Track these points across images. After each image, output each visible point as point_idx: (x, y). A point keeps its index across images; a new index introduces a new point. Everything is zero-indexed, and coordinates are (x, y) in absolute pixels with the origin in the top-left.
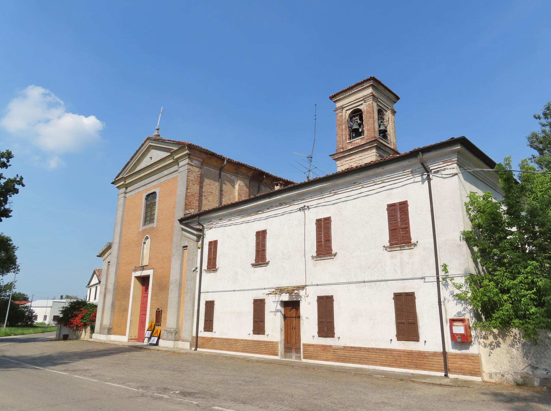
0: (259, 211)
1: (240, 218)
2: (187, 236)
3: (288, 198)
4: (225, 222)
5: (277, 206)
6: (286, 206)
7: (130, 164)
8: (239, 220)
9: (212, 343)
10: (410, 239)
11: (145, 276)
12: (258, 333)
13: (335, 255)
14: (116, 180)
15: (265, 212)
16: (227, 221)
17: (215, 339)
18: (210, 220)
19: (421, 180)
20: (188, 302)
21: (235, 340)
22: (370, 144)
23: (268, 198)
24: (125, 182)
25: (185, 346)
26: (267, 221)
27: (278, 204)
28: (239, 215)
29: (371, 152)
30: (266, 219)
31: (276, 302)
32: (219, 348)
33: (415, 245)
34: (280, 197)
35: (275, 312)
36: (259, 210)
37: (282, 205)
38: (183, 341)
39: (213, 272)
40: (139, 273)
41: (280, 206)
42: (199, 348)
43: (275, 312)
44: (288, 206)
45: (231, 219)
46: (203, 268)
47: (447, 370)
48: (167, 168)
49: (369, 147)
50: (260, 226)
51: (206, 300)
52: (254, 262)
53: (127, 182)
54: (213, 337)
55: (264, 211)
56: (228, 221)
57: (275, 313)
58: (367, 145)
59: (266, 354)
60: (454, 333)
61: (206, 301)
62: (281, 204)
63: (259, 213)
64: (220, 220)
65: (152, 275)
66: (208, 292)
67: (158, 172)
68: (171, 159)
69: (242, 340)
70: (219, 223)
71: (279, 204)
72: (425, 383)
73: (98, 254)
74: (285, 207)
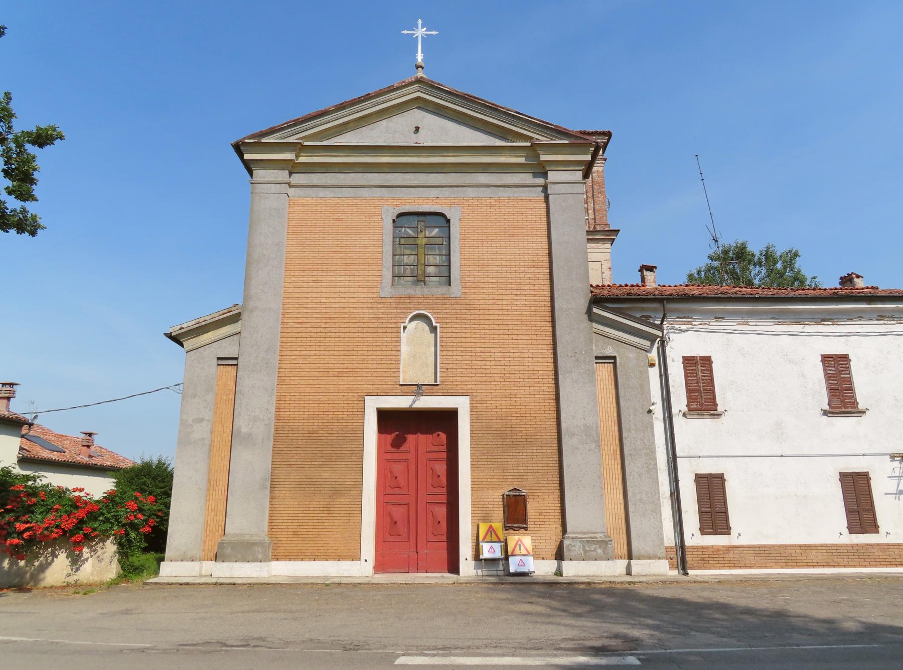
1: (772, 324)
2: (611, 336)
4: (730, 325)
5: (871, 319)
6: (889, 322)
7: (328, 118)
10: (856, 403)
11: (442, 410)
13: (719, 415)
14: (264, 140)
15: (839, 323)
16: (735, 324)
18: (686, 316)
21: (800, 546)
22: (607, 233)
23: (865, 303)
24: (297, 157)
25: (662, 569)
26: (847, 340)
27: (875, 316)
28: (772, 318)
29: (602, 246)
30: (841, 336)
31: (897, 478)
32: (757, 565)
33: (863, 412)
34: (894, 306)
35: (896, 494)
37: (883, 320)
38: (639, 559)
39: (712, 417)
41: (877, 320)
42: (693, 568)
43: (896, 494)
44: (893, 322)
45: (748, 322)
46: (675, 411)
49: (604, 237)
50: (835, 347)
52: (827, 408)
53: (302, 159)
55: (837, 322)
56: (737, 325)
57: (897, 495)
58: (602, 233)
60: (667, 561)
61: (696, 475)
63: (825, 323)
64: (716, 318)
66: (700, 457)
69: (821, 545)
70: (711, 324)
71: (878, 316)
73: (175, 330)
74: (887, 323)
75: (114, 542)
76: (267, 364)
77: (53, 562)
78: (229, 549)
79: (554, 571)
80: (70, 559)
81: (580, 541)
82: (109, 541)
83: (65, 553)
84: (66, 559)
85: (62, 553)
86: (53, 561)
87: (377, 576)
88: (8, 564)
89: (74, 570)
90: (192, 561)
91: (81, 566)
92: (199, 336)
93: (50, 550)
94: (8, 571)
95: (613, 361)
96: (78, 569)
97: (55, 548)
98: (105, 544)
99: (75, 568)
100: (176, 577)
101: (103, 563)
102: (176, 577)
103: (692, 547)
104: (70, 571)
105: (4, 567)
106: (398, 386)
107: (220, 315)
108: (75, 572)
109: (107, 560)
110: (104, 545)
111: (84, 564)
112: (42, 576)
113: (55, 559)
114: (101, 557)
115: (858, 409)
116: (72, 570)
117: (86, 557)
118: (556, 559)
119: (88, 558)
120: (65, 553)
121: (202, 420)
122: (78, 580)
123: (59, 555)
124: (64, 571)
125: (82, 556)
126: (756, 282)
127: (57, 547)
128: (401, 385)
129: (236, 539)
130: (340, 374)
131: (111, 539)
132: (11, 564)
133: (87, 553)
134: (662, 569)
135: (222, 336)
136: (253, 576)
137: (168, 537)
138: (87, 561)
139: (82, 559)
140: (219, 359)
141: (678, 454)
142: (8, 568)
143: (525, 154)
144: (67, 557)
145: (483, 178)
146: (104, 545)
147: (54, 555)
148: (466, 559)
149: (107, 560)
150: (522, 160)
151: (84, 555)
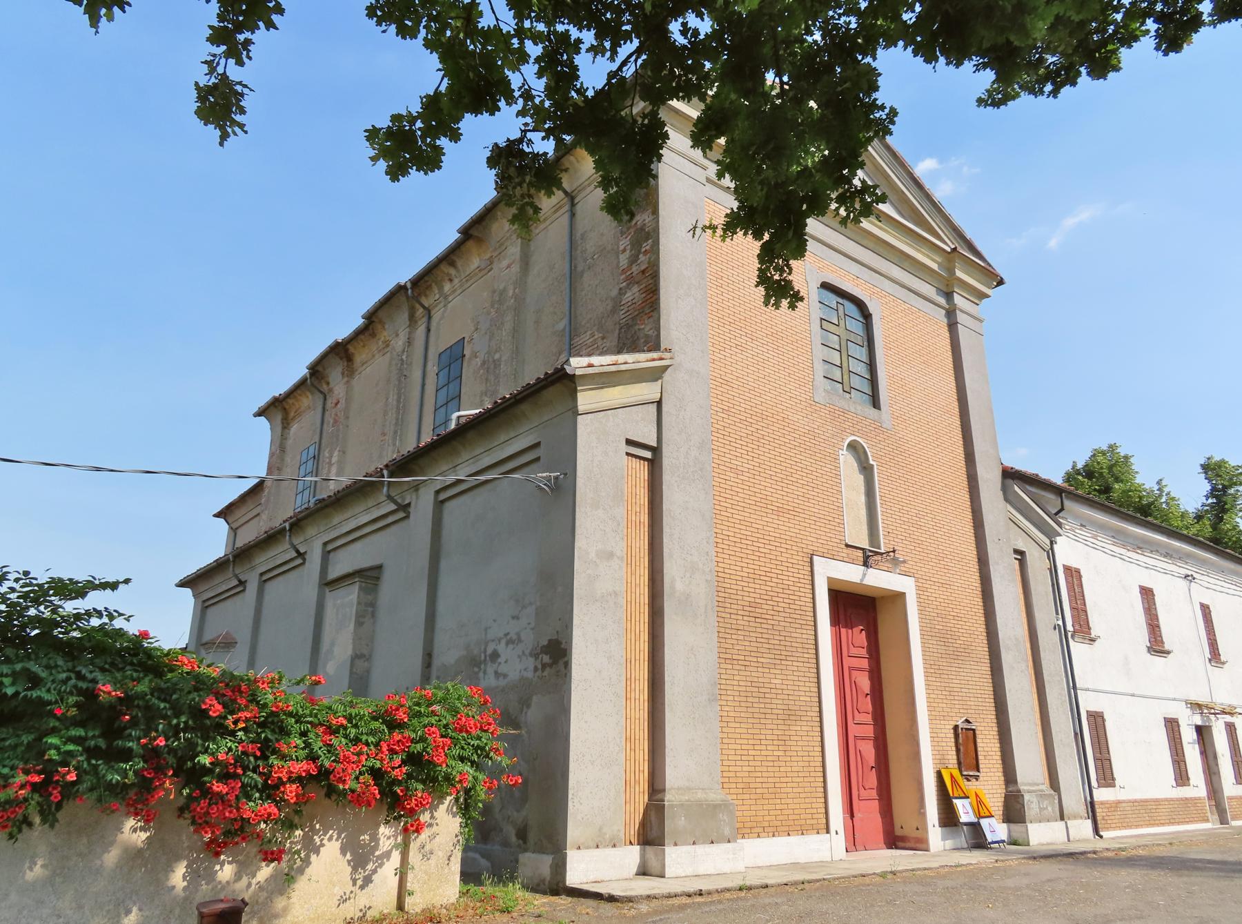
0: (1140, 548)
3: (1178, 551)
8: (1106, 543)
9: (1119, 813)
12: (1183, 785)
15: (1146, 554)
17: (1124, 805)
19: (579, 417)
20: (1057, 709)
28: (1113, 537)
33: (1168, 653)
36: (1141, 546)
40: (851, 573)
47: (1223, 820)
48: (906, 265)
51: (1166, 716)
54: (1118, 798)
59: (1197, 822)
62: (1167, 555)
64: (1082, 525)
65: (914, 592)
67: (871, 245)
68: (933, 260)
69: (1166, 800)
72: (1160, 844)
75: (455, 809)
76: (701, 470)
77: (307, 866)
78: (683, 818)
79: (635, 870)
80: (348, 856)
81: (1036, 795)
82: (443, 808)
83: (337, 840)
84: (341, 857)
85: (330, 839)
86: (307, 862)
87: (855, 856)
88: (184, 878)
89: (359, 883)
90: (614, 846)
91: (374, 871)
92: (602, 388)
93: (298, 833)
94: (186, 899)
95: (1019, 557)
96: (368, 880)
97: (312, 828)
98: (435, 814)
99: (360, 876)
100: (595, 882)
101: (432, 862)
102: (595, 882)
103: (1102, 803)
104: (349, 887)
105: (174, 887)
106: (843, 547)
107: (647, 361)
108: (362, 887)
109: (441, 854)
110: (432, 817)
111: (381, 865)
112: (280, 903)
113: (313, 857)
114: (427, 848)
115: (1164, 647)
116: (354, 884)
117: (385, 850)
118: (1003, 822)
119: (391, 850)
120: (337, 840)
121: (611, 555)
122: (370, 908)
123: (322, 845)
124: (337, 888)
125: (376, 847)
126: (1115, 495)
127: (318, 826)
128: (847, 546)
129: (687, 798)
130: (779, 511)
131: (447, 802)
132: (194, 876)
133: (389, 838)
134: (1083, 828)
135: (632, 400)
136: (725, 871)
137: (570, 796)
138: (388, 860)
139: (377, 853)
140: (629, 442)
141: (1078, 686)
142: (185, 889)
143: (939, 260)
144: (343, 851)
145: (896, 272)
146: (432, 817)
147: (312, 848)
148: (918, 829)
149: (440, 853)
150: (935, 266)
151: (381, 842)
